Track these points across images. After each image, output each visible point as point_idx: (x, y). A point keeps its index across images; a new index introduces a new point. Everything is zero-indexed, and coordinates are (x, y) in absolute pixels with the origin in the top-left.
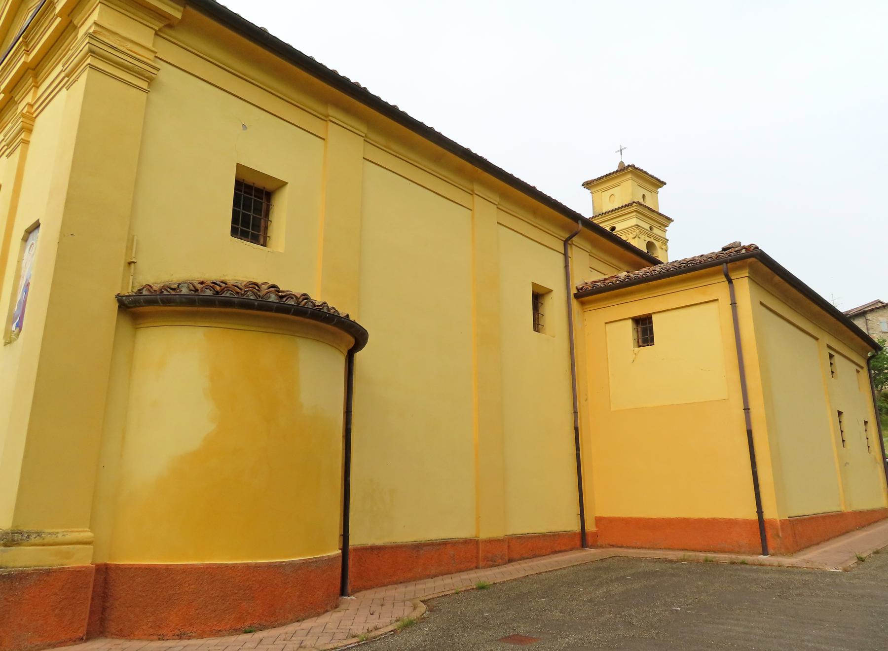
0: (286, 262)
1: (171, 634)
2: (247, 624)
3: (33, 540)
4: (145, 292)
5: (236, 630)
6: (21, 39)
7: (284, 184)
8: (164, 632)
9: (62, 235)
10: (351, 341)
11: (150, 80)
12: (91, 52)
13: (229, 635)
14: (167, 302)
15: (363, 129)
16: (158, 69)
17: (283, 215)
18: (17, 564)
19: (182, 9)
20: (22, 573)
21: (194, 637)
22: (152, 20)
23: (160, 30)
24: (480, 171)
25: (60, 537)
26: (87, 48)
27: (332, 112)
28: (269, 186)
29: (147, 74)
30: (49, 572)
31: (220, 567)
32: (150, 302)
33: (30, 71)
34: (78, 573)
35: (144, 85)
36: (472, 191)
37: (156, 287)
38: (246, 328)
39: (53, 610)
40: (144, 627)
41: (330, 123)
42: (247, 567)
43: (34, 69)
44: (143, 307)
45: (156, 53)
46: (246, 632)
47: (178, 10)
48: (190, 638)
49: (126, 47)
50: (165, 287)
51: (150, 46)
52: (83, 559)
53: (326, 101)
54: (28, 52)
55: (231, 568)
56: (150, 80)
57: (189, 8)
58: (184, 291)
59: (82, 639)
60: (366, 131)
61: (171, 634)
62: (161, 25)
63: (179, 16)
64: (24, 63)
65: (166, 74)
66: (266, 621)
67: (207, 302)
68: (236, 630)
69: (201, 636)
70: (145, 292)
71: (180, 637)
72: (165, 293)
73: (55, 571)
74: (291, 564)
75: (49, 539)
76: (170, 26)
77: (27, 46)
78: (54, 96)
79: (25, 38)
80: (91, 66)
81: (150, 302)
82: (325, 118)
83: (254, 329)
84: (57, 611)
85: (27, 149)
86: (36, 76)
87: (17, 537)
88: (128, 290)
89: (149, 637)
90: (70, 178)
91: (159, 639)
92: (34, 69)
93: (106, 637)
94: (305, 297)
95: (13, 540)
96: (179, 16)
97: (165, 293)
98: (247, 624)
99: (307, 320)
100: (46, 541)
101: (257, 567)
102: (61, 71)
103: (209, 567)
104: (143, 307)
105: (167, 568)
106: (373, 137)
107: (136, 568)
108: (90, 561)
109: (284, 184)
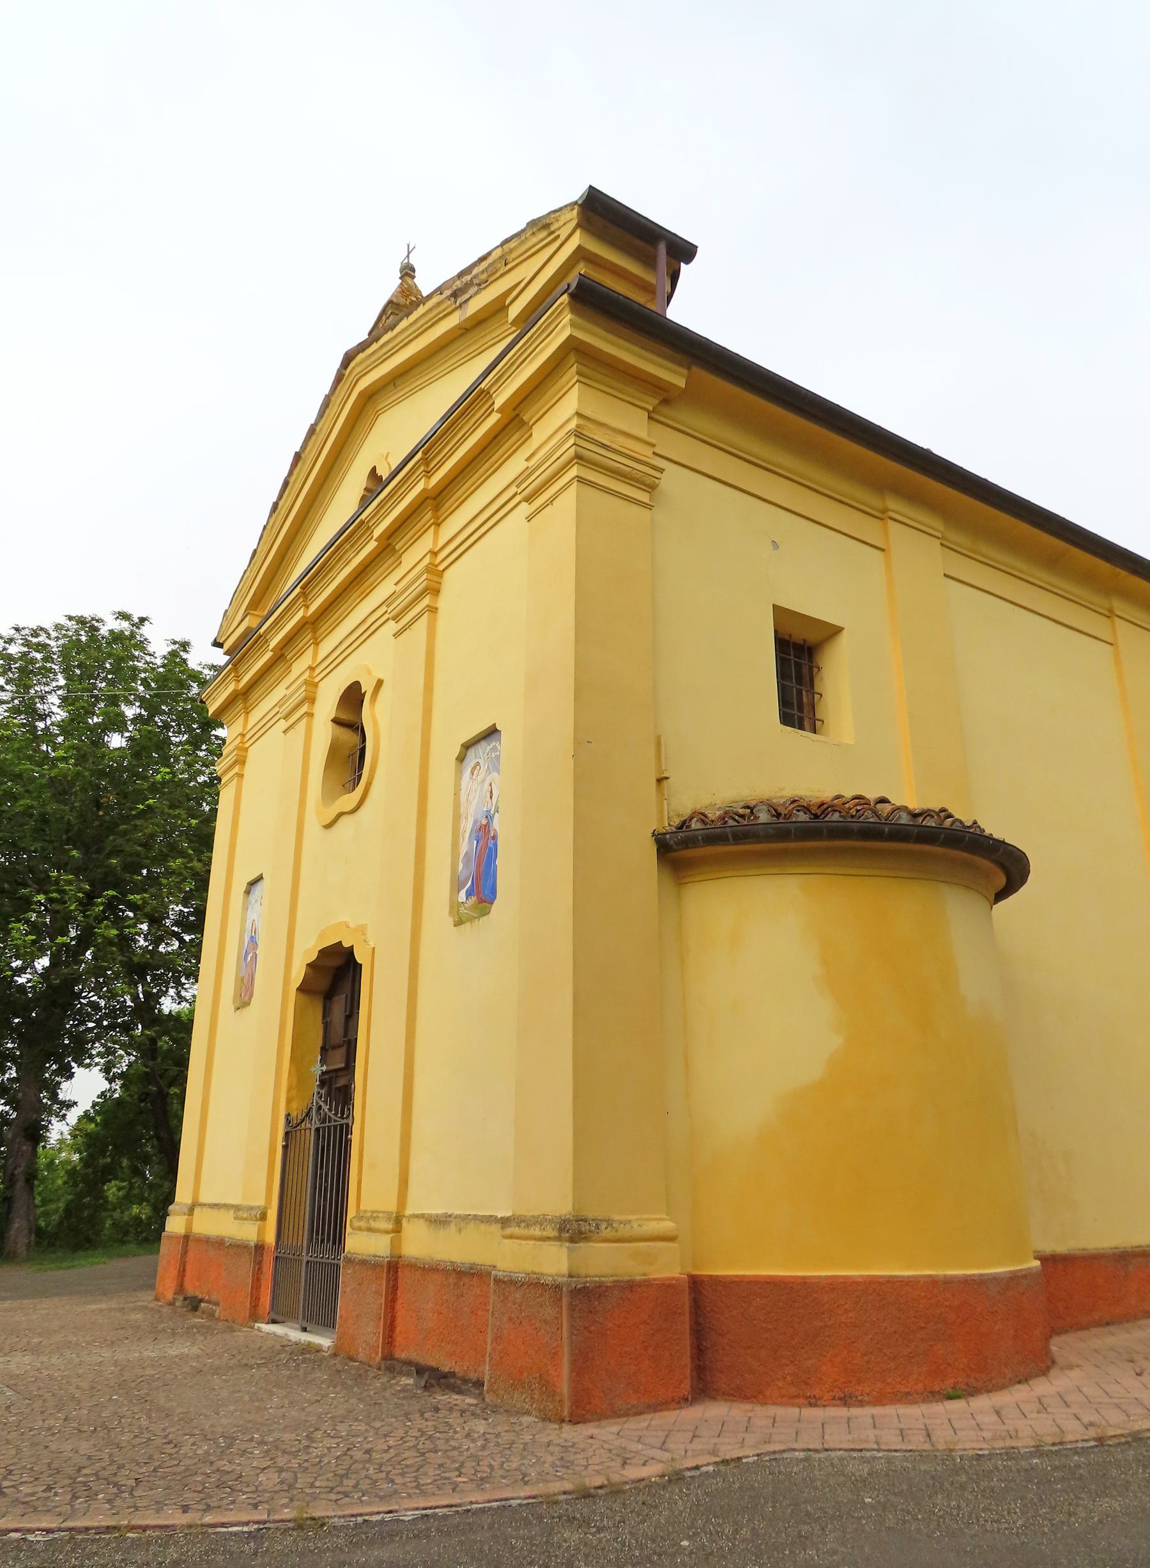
0: (858, 756)
1: (827, 1396)
2: (949, 1382)
3: (605, 1232)
4: (695, 825)
5: (933, 1393)
6: (419, 455)
7: (836, 631)
8: (817, 1392)
9: (577, 742)
10: (1001, 880)
11: (651, 488)
12: (578, 457)
13: (924, 1401)
14: (741, 836)
15: (936, 524)
16: (662, 471)
17: (839, 679)
18: (592, 1272)
19: (685, 371)
20: (600, 1285)
21: (869, 1403)
22: (644, 397)
23: (654, 411)
24: (1123, 573)
25: (637, 1230)
26: (572, 451)
27: (894, 504)
28: (812, 637)
29: (649, 480)
30: (631, 1286)
31: (891, 1281)
32: (712, 839)
33: (429, 501)
34: (667, 1287)
35: (643, 497)
36: (1111, 611)
37: (713, 814)
38: (866, 872)
39: (646, 1349)
40: (780, 1384)
41: (891, 523)
42: (933, 1281)
43: (435, 499)
44: (695, 848)
45: (654, 445)
46: (950, 1398)
47: (680, 374)
48: (861, 1404)
49: (619, 442)
50: (728, 814)
51: (643, 435)
52: (668, 1266)
53: (882, 486)
54: (428, 474)
55: (907, 1284)
56: (651, 488)
57: (695, 369)
58: (764, 817)
59: (687, 1400)
60: (942, 528)
61: (827, 1396)
62: (657, 402)
63: (681, 383)
64: (424, 490)
65: (673, 480)
66: (976, 1379)
67: (840, 832)
68: (933, 1393)
69: (879, 1401)
70: (695, 825)
71: (845, 1401)
72: (731, 823)
73: (640, 1284)
74: (995, 1278)
75: (624, 1231)
76: (666, 402)
77: (427, 465)
78: (459, 532)
79: (425, 453)
80: (580, 480)
81: (712, 839)
82: (881, 516)
83: (877, 872)
84: (650, 1351)
85: (435, 620)
86: (436, 509)
87: (585, 1227)
88: (667, 824)
89: (790, 1400)
90: (576, 652)
91: (811, 1405)
92: (435, 499)
93: (713, 1398)
94: (944, 813)
95: (581, 1233)
96: (681, 383)
97: (731, 823)
98: (949, 1382)
99: (792, 845)
100: (620, 1234)
101: (948, 1281)
102: (516, 494)
103: (873, 1281)
104: (695, 848)
105: (804, 1282)
106: (954, 537)
107: (750, 1282)
108: (678, 1270)
109: (836, 631)
